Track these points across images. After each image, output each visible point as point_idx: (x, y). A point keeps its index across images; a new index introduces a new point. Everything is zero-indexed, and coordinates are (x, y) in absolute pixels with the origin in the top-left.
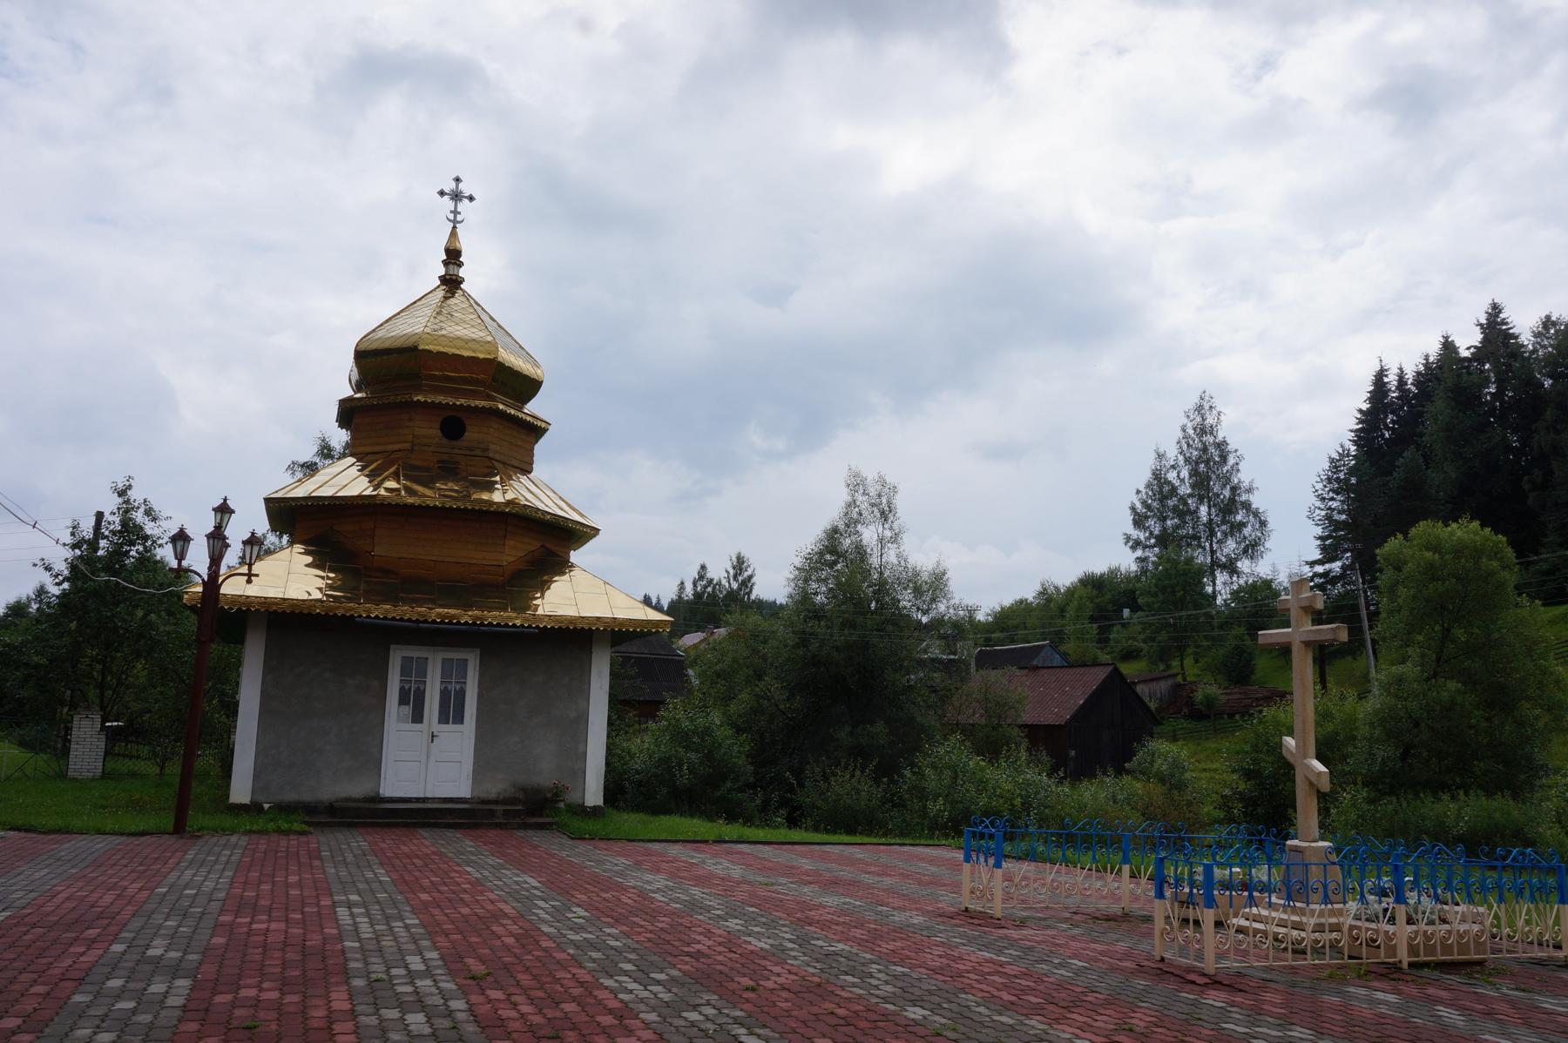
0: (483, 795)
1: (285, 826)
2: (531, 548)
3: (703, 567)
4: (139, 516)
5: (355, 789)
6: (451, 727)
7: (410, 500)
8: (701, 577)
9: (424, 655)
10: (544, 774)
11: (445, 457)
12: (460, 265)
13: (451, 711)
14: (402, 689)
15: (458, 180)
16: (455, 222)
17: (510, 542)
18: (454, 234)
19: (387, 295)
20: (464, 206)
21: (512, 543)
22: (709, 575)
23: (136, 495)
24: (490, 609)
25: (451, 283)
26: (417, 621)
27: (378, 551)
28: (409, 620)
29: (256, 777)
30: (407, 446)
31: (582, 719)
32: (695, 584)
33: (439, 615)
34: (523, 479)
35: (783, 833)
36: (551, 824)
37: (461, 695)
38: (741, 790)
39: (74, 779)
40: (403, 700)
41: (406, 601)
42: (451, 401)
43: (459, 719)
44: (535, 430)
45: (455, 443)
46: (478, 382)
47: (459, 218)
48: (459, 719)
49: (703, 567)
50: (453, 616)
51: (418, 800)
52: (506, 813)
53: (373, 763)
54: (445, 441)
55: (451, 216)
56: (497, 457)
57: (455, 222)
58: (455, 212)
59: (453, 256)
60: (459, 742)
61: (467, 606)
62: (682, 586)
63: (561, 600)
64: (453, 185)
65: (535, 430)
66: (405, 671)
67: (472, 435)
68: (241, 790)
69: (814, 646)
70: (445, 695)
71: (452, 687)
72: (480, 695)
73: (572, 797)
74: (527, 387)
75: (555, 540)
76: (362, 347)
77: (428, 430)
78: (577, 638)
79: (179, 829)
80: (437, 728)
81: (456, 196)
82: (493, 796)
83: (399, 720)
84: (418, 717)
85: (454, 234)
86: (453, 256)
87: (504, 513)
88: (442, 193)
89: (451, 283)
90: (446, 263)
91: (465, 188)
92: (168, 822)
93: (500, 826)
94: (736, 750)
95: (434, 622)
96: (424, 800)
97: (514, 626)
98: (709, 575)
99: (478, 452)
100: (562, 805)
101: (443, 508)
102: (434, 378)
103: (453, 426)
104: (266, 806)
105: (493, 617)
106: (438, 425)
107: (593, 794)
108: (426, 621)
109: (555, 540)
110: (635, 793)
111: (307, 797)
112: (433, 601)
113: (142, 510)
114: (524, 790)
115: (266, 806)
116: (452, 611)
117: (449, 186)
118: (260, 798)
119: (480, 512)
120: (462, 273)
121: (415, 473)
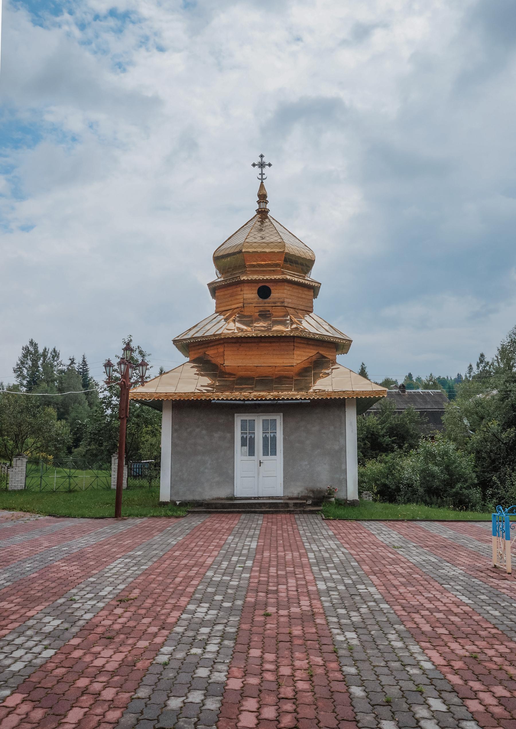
0: (290, 495)
1: (170, 513)
2: (311, 355)
3: (482, 355)
4: (136, 355)
5: (220, 493)
6: (270, 457)
7: (240, 334)
8: (482, 362)
9: (274, 418)
10: (323, 481)
11: (261, 309)
12: (266, 202)
13: (270, 447)
14: (242, 438)
15: (262, 156)
16: (262, 179)
17: (297, 352)
18: (262, 186)
19: (225, 225)
20: (266, 170)
21: (298, 352)
22: (486, 360)
23: (133, 345)
24: (283, 390)
25: (263, 214)
26: (244, 400)
27: (227, 363)
28: (240, 400)
29: (172, 487)
30: (241, 305)
31: (343, 449)
32: (478, 366)
33: (255, 396)
34: (307, 318)
35: (452, 514)
36: (318, 511)
37: (274, 439)
38: (468, 488)
39: (14, 491)
40: (243, 444)
41: (237, 390)
42: (261, 277)
43: (274, 453)
44: (313, 289)
45: (266, 300)
46: (277, 265)
47: (264, 177)
48: (274, 453)
49: (482, 355)
50: (263, 396)
51: (255, 498)
52: (295, 504)
53: (230, 479)
54: (261, 300)
55: (260, 177)
56: (290, 305)
57: (262, 179)
58: (262, 174)
59: (262, 197)
60: (275, 464)
61: (270, 390)
62: (470, 368)
63: (326, 385)
64: (259, 159)
65: (313, 289)
66: (243, 428)
67: (276, 294)
68: (165, 494)
69: (496, 398)
70: (265, 439)
71: (268, 435)
72: (284, 439)
73: (340, 495)
74: (304, 264)
75: (327, 349)
76: (216, 255)
77: (250, 294)
78: (334, 405)
79: (117, 515)
80: (262, 458)
81: (262, 165)
82: (295, 495)
83: (242, 454)
84: (252, 453)
85: (262, 186)
86: (262, 197)
87: (290, 337)
88: (270, 165)
89: (263, 214)
90: (259, 202)
91: (266, 160)
92: (113, 510)
93: (290, 512)
94: (465, 464)
95: (253, 400)
96: (258, 498)
97: (296, 399)
98: (486, 360)
99: (279, 304)
100: (333, 499)
101: (257, 337)
102: (254, 266)
103: (264, 292)
104: (178, 503)
105: (284, 394)
106: (256, 292)
107: (352, 492)
108: (248, 400)
109: (327, 349)
110: (387, 493)
111: (197, 498)
112: (252, 389)
113: (137, 352)
114: (313, 491)
115: (178, 503)
116: (262, 393)
117: (257, 160)
118: (175, 498)
119: (277, 337)
120: (268, 206)
121: (246, 319)
